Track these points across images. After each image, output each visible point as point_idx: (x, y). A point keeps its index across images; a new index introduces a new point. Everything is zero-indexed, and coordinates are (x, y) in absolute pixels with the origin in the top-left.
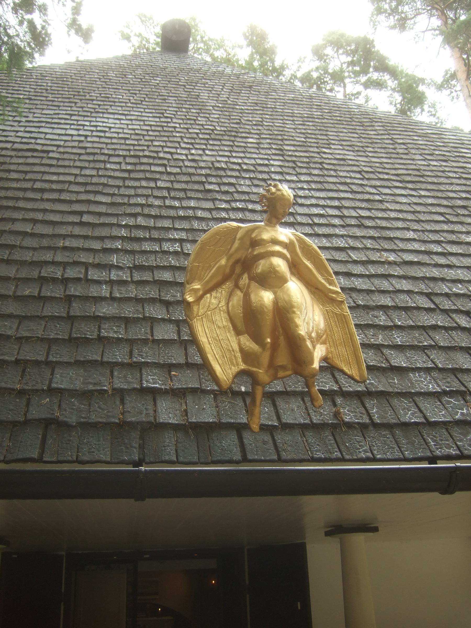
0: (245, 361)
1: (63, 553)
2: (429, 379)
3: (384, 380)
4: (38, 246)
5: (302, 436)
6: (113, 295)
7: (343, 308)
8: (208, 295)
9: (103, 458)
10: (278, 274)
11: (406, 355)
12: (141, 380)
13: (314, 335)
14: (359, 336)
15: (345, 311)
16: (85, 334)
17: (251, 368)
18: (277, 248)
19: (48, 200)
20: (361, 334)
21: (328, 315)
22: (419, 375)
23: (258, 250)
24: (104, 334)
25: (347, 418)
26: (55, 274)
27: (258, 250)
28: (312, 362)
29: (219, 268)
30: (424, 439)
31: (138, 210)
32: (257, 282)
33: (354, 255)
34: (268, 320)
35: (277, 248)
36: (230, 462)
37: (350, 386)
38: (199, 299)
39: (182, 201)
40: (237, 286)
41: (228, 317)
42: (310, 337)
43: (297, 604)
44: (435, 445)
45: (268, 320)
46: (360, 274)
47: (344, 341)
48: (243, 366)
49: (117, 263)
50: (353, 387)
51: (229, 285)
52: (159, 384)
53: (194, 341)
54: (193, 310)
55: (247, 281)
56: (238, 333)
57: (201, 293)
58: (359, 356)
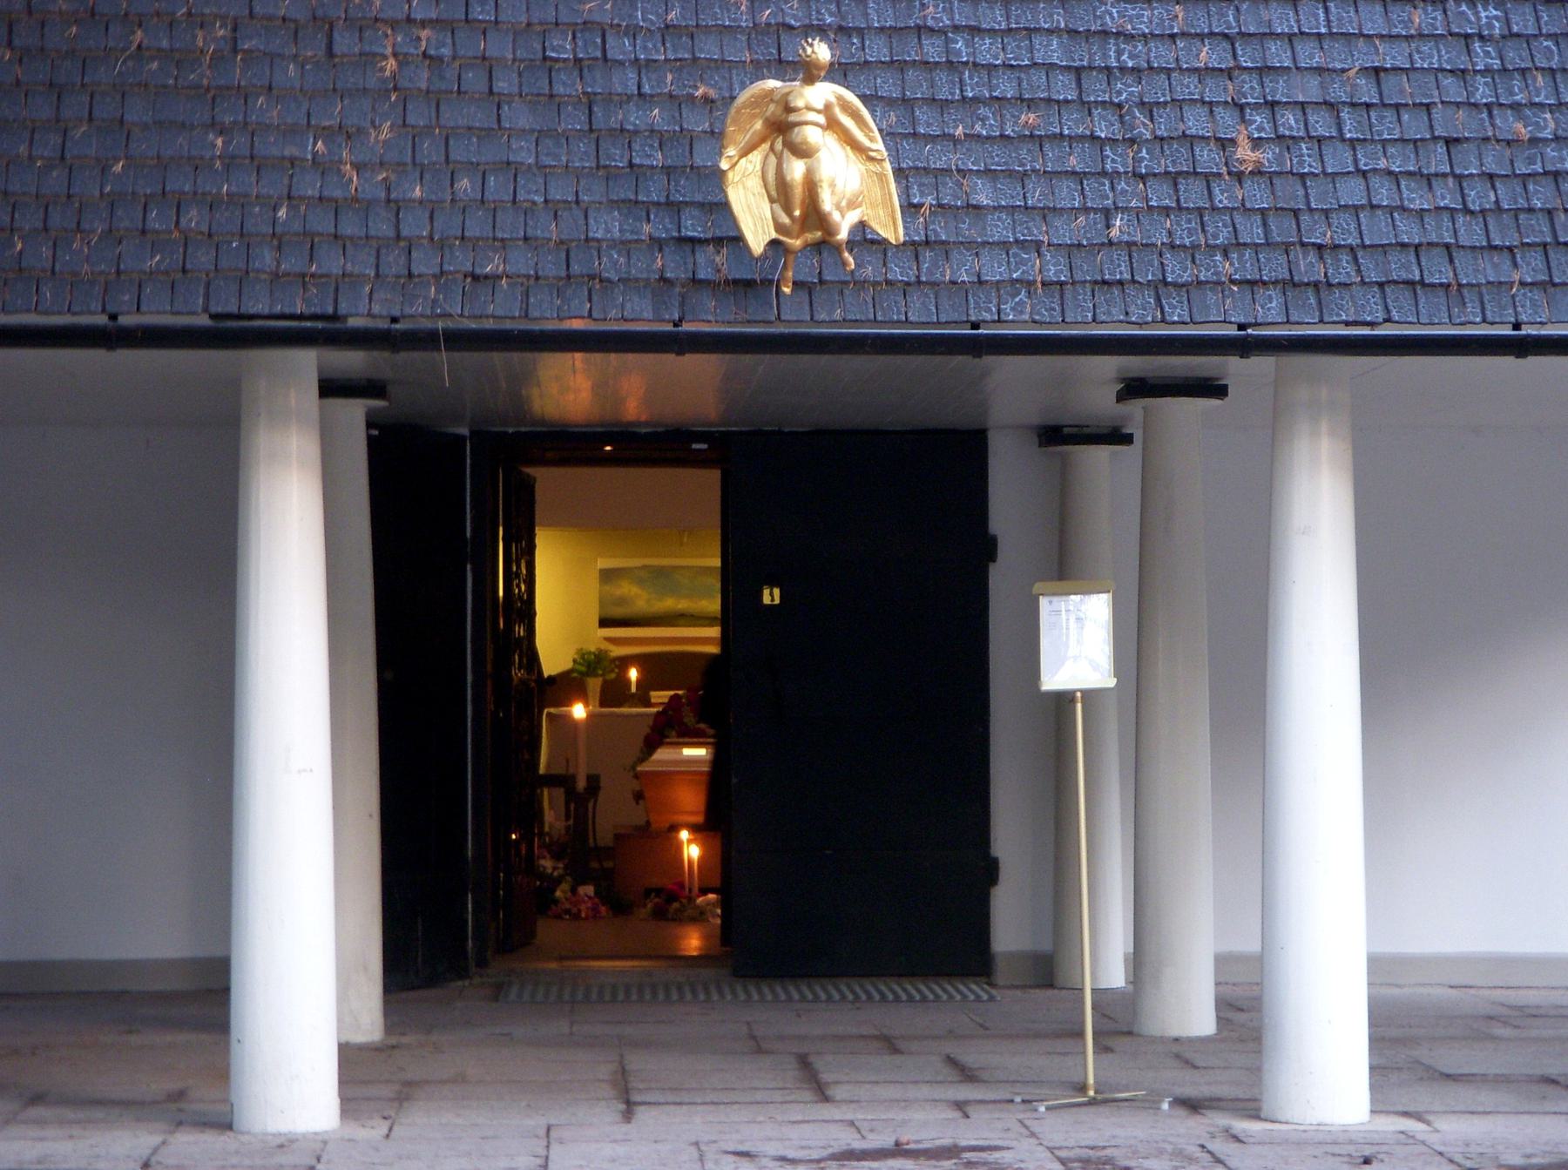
0: (777, 230)
1: (464, 431)
3: (952, 224)
6: (671, 198)
9: (645, 315)
11: (995, 186)
12: (679, 227)
18: (811, 116)
23: (793, 118)
29: (754, 133)
34: (798, 193)
35: (811, 116)
36: (1371, 324)
38: (733, 166)
39: (697, 247)
40: (772, 149)
43: (704, 443)
45: (798, 193)
48: (774, 235)
51: (766, 146)
53: (725, 206)
55: (781, 148)
56: (772, 201)
57: (736, 159)
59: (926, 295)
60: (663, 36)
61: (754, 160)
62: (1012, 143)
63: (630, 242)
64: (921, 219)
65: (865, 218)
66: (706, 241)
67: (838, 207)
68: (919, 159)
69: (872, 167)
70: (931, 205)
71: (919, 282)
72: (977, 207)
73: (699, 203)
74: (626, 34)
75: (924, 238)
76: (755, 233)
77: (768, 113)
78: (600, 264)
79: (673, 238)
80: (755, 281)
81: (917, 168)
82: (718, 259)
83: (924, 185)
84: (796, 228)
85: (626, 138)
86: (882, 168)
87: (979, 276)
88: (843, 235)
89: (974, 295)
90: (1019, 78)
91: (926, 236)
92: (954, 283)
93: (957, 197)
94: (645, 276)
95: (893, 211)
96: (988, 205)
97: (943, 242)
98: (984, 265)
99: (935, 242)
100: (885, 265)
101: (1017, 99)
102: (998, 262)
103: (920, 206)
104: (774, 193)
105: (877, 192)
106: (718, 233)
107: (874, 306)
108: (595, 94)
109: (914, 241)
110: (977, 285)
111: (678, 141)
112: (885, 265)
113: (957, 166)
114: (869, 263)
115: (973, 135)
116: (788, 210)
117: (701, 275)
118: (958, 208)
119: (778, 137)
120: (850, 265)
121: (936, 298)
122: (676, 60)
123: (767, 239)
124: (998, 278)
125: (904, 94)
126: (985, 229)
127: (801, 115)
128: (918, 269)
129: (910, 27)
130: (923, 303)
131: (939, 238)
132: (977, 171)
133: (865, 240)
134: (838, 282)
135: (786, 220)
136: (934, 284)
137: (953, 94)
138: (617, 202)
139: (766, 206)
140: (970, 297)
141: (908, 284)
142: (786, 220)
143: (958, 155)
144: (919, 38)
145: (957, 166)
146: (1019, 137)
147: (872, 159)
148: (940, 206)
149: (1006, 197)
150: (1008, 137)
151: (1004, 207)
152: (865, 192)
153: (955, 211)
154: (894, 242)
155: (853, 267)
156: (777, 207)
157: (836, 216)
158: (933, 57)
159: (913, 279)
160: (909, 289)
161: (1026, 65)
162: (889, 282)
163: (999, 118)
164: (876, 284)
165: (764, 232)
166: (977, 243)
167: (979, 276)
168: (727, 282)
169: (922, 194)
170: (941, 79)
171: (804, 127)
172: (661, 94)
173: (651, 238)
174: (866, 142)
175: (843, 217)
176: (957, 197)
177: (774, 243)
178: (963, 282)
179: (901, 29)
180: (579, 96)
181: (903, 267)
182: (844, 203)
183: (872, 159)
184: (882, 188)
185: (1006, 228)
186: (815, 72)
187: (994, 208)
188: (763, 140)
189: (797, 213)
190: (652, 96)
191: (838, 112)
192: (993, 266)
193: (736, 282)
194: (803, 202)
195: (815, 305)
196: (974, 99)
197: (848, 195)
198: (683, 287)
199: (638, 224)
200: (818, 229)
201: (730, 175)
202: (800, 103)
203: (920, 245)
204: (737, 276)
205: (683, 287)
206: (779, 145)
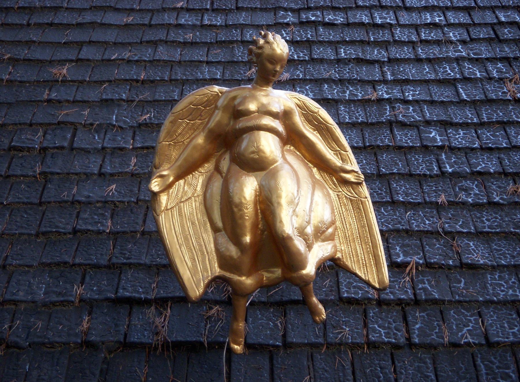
2: (513, 283)
3: (444, 283)
4: (14, 100)
5: (310, 359)
7: (360, 192)
8: (182, 182)
10: (263, 154)
11: (490, 247)
13: (309, 230)
14: (429, 220)
15: (363, 196)
16: (57, 227)
17: (228, 275)
18: (267, 121)
19: (39, 25)
20: (433, 217)
21: (340, 201)
22: (499, 276)
23: (242, 123)
24: (81, 226)
25: (373, 337)
26: (30, 142)
27: (242, 123)
28: (303, 266)
30: (475, 366)
31: (161, 35)
32: (238, 164)
33: (464, 90)
35: (267, 121)
37: (391, 293)
40: (217, 169)
41: (204, 211)
42: (302, 233)
44: (487, 374)
46: (463, 123)
47: (360, 237)
48: (217, 271)
49: (116, 121)
50: (396, 293)
51: (208, 167)
52: (511, 251)
54: (160, 202)
56: (215, 230)
57: (171, 179)
58: (379, 255)
59: (421, 360)
60: (134, 133)
61: (194, 182)
62: (502, 210)
63: (54, 304)
64: (408, 279)
65: (339, 255)
66: (147, 303)
67: (302, 233)
68: (400, 223)
69: (345, 191)
70: (417, 264)
71: (411, 345)
72: (473, 267)
73: (145, 265)
74: (97, 131)
75: (412, 297)
76: (194, 271)
77: (212, 124)
78: (10, 328)
79: (108, 299)
80: (201, 344)
81: (398, 231)
82: (157, 320)
83: (408, 246)
84: (247, 260)
85: (76, 208)
86: (359, 194)
87: (487, 338)
88: (310, 270)
89: (483, 360)
90: (499, 158)
91: (415, 294)
92: (455, 345)
93: (446, 256)
94: (64, 339)
95: (374, 246)
96: (485, 264)
97: (435, 302)
98: (491, 325)
99: (426, 301)
100: (365, 325)
101: (500, 173)
102: (508, 322)
103: (405, 265)
104: (220, 224)
105: (352, 220)
106: (163, 294)
107: (354, 373)
108: (52, 173)
109: (400, 300)
110: (486, 348)
111: (131, 210)
112: (365, 325)
113: (443, 229)
114: (346, 323)
115: (457, 203)
116: (236, 239)
117: (134, 338)
118: (449, 268)
119: (225, 153)
120: (319, 314)
121: (434, 363)
122: (142, 148)
123: (210, 276)
124: (512, 339)
125: (379, 170)
126: (485, 287)
127: (252, 119)
128: (408, 331)
129: (383, 122)
130: (419, 369)
131: (431, 297)
132: (467, 233)
133: (341, 299)
134: (306, 345)
135: (233, 251)
136: (430, 347)
137: (431, 170)
138: (49, 265)
139: (208, 237)
140: (479, 361)
141: (396, 347)
142: (233, 251)
143: (443, 220)
144: (392, 131)
145: (443, 229)
146: (510, 204)
147: (345, 182)
148: (429, 265)
149: (505, 257)
150: (497, 204)
151: (504, 266)
152: (338, 224)
153: (446, 271)
154: (377, 286)
155: (324, 316)
156: (223, 239)
157: (299, 244)
158: (407, 143)
159: (402, 340)
160: (398, 353)
161: (505, 148)
162: (372, 345)
163: (483, 189)
164: (354, 346)
165: (205, 269)
166: (478, 301)
167: (487, 338)
168: (166, 345)
169: (406, 254)
170: (417, 160)
171: (262, 133)
172: (121, 173)
173: (81, 300)
174: (337, 162)
175: (309, 247)
176: (446, 256)
177: (217, 280)
178: (468, 344)
179: (372, 124)
180: (35, 177)
181: (389, 328)
182: (309, 230)
183: (345, 182)
184: (359, 219)
185: (511, 287)
186: (270, 66)
187: (493, 267)
188: (205, 159)
189: (248, 239)
190: (112, 175)
191: (298, 120)
192: (502, 327)
193: (178, 345)
194: (255, 226)
195: (277, 372)
196: (454, 174)
197: (314, 221)
198: (110, 352)
199: (68, 286)
200: (277, 266)
201: (164, 198)
202: (253, 107)
203: (408, 304)
204: (180, 339)
205: (110, 352)
206: (225, 164)
